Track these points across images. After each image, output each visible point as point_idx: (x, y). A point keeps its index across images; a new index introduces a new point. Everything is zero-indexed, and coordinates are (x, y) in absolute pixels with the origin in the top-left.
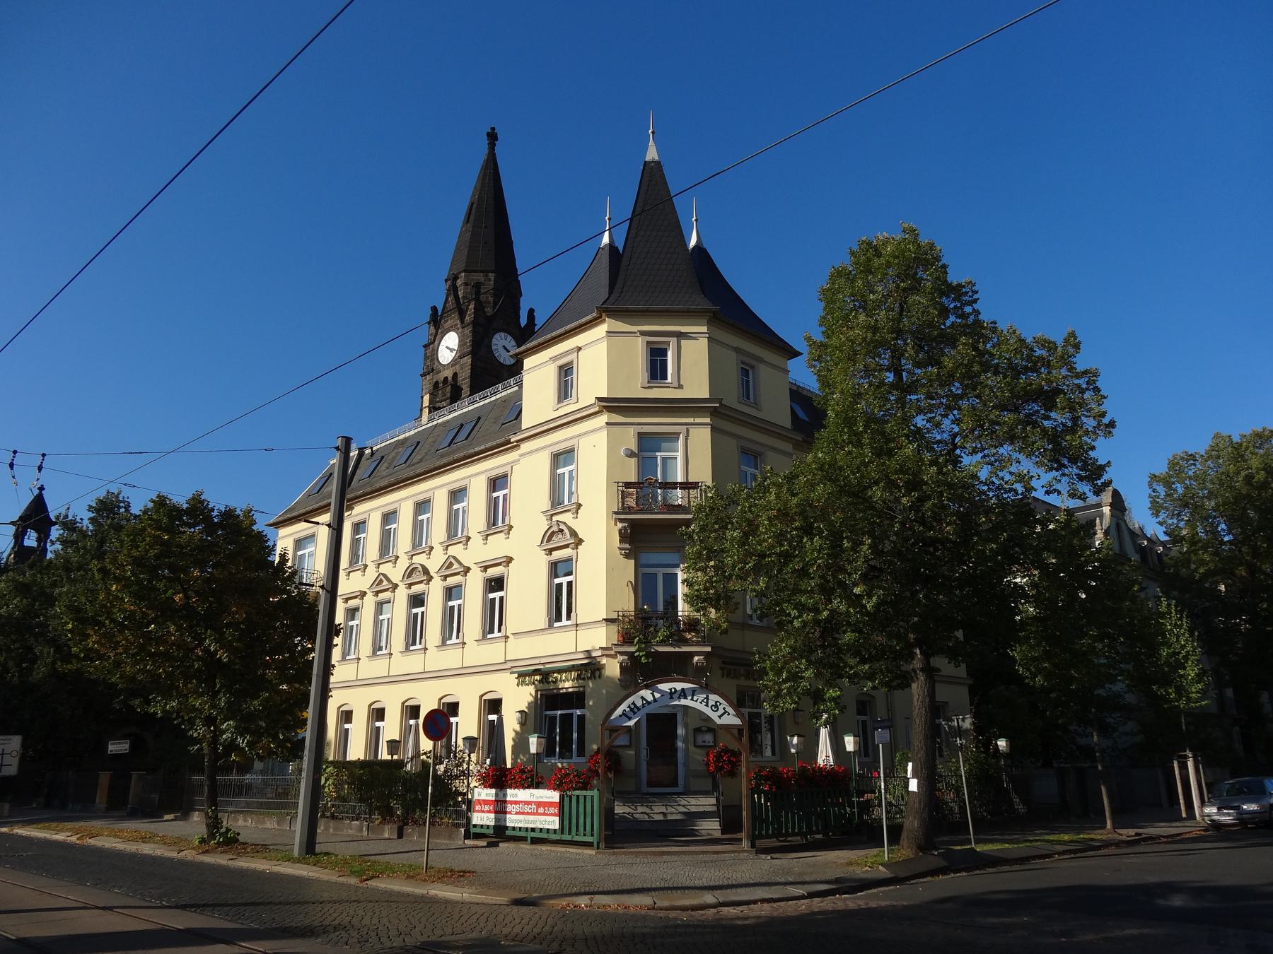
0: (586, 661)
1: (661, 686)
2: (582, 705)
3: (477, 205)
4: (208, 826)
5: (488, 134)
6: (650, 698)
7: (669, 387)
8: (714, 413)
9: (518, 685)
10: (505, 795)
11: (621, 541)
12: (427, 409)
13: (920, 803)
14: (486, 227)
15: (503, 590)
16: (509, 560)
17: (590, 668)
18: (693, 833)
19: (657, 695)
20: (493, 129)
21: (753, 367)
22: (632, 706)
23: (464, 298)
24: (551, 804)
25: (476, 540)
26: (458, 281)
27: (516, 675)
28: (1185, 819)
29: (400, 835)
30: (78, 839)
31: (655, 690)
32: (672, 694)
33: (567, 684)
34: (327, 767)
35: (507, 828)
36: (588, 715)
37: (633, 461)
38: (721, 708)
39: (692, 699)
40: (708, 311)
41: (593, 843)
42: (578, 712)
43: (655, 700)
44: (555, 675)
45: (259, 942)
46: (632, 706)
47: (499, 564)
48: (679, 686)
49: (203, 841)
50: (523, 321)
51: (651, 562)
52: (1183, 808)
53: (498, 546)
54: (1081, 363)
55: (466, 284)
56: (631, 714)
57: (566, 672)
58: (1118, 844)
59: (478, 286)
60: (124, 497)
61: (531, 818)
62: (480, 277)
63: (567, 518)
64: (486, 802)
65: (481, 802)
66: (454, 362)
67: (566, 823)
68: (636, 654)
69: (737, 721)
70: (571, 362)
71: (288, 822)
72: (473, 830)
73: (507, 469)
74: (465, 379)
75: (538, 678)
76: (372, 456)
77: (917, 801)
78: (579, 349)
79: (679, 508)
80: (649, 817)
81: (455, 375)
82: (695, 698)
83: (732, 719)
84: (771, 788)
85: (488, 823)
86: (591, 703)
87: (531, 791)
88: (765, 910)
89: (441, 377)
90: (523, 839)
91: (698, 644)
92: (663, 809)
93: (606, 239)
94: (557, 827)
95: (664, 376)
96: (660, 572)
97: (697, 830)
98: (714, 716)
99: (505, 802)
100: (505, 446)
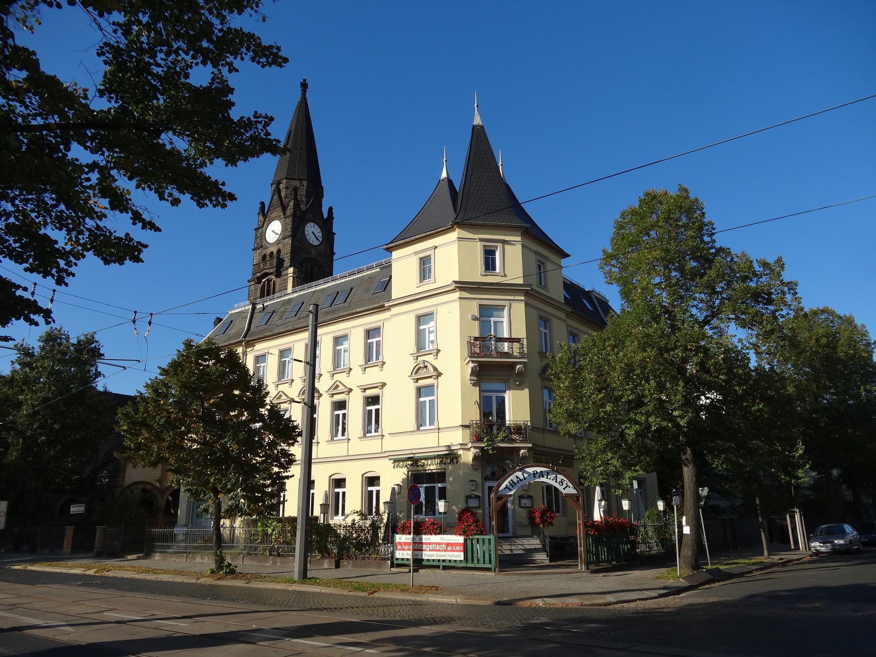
0: (446, 452)
1: (527, 470)
2: (444, 481)
3: (295, 132)
4: (216, 562)
5: (302, 84)
6: (522, 477)
7: (498, 275)
8: (527, 293)
9: (394, 467)
10: (421, 539)
11: (471, 375)
12: (291, 278)
13: (692, 541)
14: (301, 149)
15: (379, 404)
16: (384, 384)
17: (450, 456)
18: (532, 561)
19: (526, 475)
20: (305, 80)
21: (543, 264)
22: (511, 482)
23: (286, 197)
24: (457, 544)
25: (357, 371)
26: (281, 185)
27: (392, 461)
28: (793, 550)
29: (338, 566)
30: (95, 573)
31: (524, 472)
32: (535, 474)
33: (432, 467)
34: (272, 522)
35: (423, 560)
36: (448, 487)
37: (477, 323)
38: (564, 483)
39: (547, 478)
40: (522, 227)
41: (491, 568)
42: (440, 485)
43: (525, 478)
44: (423, 461)
45: (57, 646)
46: (511, 482)
47: (376, 387)
48: (539, 469)
49: (213, 572)
50: (326, 216)
51: (488, 389)
52: (792, 543)
53: (373, 376)
54: (786, 276)
55: (287, 188)
56: (511, 487)
57: (431, 459)
58: (773, 565)
59: (296, 189)
60: (64, 331)
61: (442, 553)
62: (297, 183)
63: (430, 358)
64: (405, 544)
65: (402, 544)
66: (278, 242)
67: (470, 556)
68: (485, 448)
69: (575, 492)
70: (430, 256)
71: (241, 559)
72: (395, 562)
73: (380, 324)
74: (287, 254)
75: (410, 463)
76: (263, 310)
77: (690, 539)
78: (436, 247)
79: (506, 355)
80: (502, 552)
81: (279, 251)
82: (549, 477)
83: (571, 490)
84: (594, 533)
85: (408, 557)
86: (451, 479)
87: (441, 536)
88: (641, 605)
89: (268, 252)
90: (438, 567)
91: (522, 442)
92: (509, 547)
93: (444, 174)
94: (462, 558)
95: (494, 269)
96: (494, 395)
97: (535, 560)
98: (560, 488)
99: (422, 543)
100: (381, 309)
